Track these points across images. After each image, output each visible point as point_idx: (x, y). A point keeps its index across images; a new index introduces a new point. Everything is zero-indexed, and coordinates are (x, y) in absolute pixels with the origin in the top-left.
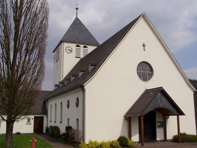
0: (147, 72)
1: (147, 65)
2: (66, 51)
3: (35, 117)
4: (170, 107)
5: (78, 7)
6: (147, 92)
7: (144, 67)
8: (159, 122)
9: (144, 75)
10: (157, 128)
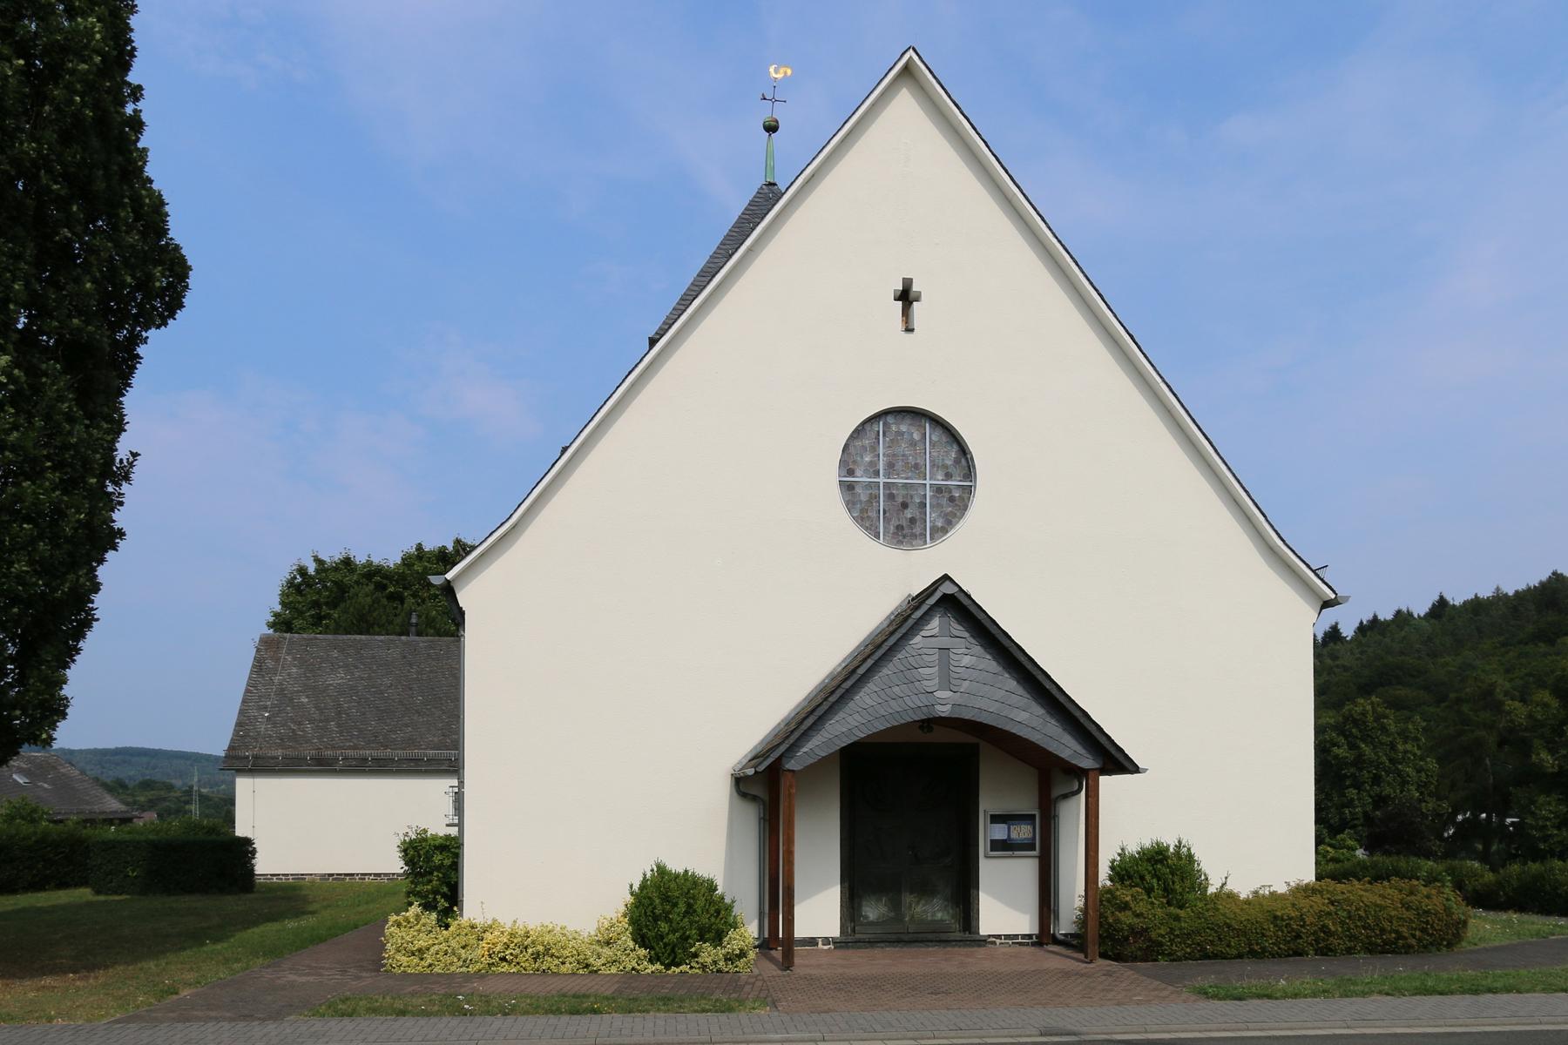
0: (928, 482)
1: (890, 419)
4: (1022, 716)
5: (781, 114)
7: (903, 447)
8: (996, 819)
9: (905, 506)
10: (987, 857)
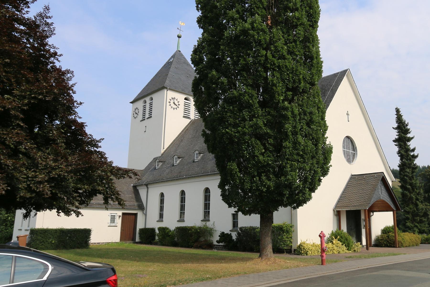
2: (170, 105)
3: (123, 214)
5: (181, 34)
6: (353, 177)
